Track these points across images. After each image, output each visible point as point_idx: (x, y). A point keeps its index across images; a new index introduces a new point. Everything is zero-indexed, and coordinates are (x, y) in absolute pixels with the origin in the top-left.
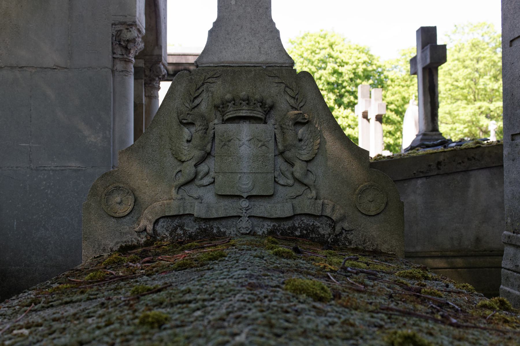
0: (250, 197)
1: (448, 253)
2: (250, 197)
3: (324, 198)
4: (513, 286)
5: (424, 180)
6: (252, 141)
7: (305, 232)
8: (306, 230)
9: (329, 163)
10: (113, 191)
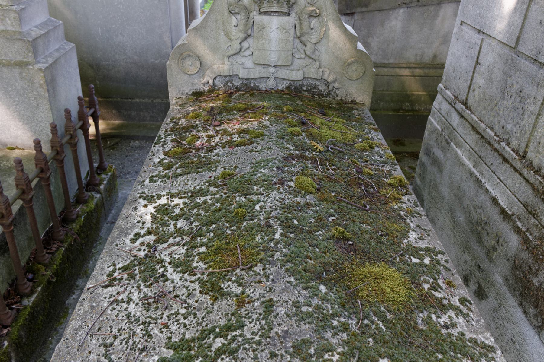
0: (275, 66)
1: (411, 65)
2: (275, 66)
3: (324, 67)
4: (435, 119)
5: (406, 9)
6: (279, 29)
7: (309, 88)
8: (310, 87)
9: (330, 44)
10: (186, 57)
